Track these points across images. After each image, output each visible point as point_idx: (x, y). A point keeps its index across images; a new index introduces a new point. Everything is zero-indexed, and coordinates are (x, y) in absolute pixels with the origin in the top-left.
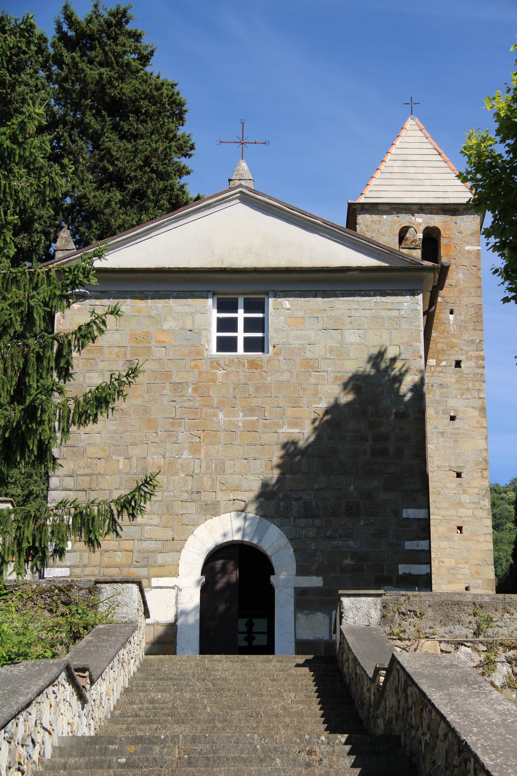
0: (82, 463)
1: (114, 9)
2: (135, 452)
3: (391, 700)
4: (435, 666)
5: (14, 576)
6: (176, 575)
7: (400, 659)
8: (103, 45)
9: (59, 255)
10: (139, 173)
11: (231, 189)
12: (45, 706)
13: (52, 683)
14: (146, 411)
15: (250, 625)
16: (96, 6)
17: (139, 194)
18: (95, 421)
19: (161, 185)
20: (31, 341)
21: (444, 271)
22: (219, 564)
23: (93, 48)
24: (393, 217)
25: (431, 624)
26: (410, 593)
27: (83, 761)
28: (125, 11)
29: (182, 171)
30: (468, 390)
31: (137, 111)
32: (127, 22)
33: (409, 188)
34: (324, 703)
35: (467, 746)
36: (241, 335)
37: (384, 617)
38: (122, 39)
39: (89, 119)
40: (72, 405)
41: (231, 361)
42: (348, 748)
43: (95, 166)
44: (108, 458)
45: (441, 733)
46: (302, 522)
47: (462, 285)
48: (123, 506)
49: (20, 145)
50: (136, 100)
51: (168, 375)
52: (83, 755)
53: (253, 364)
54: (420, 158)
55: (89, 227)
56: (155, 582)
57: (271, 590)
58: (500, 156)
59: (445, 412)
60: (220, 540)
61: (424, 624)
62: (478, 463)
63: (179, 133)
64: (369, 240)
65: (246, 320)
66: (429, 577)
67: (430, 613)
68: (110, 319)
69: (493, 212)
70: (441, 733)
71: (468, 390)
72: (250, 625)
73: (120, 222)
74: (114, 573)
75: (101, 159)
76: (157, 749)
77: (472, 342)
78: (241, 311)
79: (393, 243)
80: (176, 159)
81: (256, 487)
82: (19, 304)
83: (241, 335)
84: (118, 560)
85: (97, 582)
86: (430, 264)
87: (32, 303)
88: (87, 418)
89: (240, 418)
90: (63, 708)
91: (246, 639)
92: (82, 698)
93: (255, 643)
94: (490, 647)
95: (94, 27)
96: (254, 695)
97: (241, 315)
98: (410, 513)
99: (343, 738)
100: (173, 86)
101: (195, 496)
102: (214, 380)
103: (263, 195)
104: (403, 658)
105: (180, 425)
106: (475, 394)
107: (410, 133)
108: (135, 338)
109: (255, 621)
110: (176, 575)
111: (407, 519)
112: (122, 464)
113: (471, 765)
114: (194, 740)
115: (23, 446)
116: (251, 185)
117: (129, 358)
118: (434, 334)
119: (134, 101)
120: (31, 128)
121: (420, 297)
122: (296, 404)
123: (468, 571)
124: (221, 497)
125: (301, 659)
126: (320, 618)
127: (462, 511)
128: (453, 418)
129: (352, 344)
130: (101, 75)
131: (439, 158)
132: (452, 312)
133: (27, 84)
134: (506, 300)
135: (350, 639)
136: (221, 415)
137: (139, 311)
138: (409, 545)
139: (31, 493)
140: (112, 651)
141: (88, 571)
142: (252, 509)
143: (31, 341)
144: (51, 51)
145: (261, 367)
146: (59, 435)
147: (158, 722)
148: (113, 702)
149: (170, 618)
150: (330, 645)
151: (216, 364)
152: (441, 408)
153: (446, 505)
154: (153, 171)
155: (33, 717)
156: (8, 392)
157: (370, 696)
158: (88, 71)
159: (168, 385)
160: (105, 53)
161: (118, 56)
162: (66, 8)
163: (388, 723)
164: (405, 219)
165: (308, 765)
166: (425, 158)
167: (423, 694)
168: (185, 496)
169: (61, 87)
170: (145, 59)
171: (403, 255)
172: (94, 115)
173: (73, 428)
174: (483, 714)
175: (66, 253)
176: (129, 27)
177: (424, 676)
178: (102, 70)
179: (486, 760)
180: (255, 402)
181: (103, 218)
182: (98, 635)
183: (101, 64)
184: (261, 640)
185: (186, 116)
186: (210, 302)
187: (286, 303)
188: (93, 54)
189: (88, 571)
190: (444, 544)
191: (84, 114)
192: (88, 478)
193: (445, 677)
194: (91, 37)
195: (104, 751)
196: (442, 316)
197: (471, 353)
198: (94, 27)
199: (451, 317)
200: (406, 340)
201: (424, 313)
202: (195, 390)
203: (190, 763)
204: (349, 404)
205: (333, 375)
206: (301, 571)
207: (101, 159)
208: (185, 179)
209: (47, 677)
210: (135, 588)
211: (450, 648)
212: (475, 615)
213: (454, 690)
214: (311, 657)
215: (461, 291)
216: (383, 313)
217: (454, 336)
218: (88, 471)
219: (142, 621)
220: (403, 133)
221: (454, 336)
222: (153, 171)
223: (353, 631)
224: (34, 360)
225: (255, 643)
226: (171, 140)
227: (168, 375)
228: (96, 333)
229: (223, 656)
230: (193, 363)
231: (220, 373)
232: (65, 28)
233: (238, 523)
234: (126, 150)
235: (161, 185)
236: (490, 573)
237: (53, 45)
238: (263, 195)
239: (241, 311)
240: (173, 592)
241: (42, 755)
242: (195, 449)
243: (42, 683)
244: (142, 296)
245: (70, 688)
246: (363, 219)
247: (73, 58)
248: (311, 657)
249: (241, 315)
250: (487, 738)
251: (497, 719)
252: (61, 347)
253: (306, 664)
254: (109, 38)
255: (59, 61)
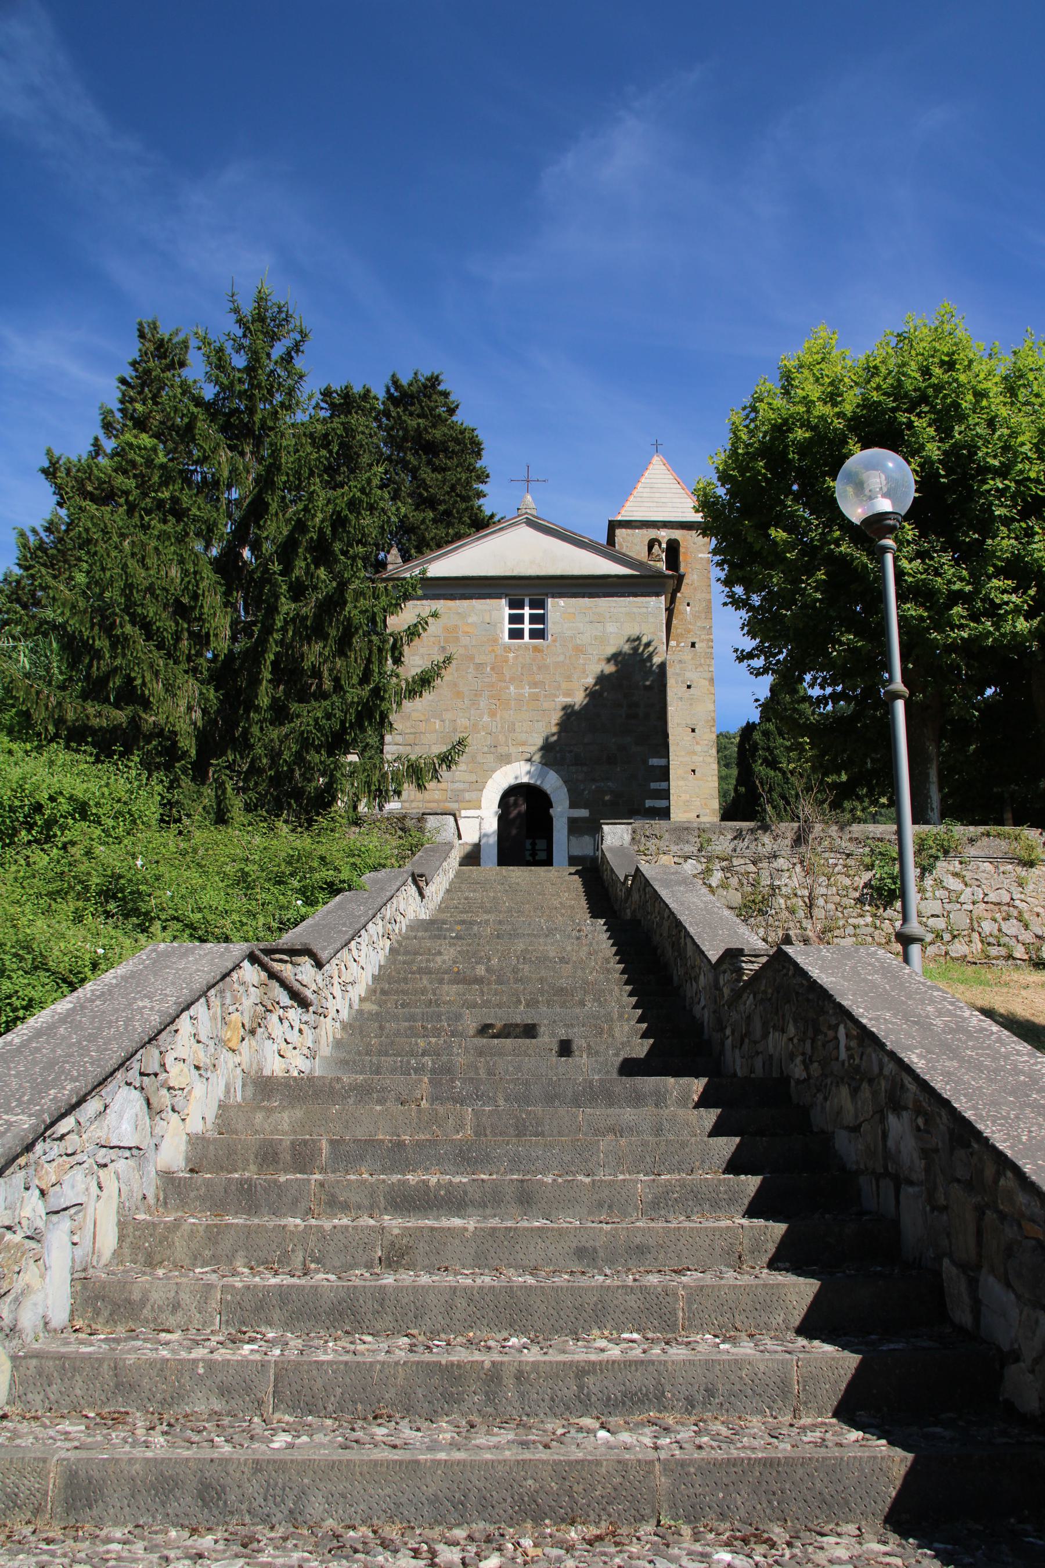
0: (408, 724)
1: (429, 375)
2: (448, 716)
3: (635, 896)
4: (665, 873)
5: (366, 809)
6: (479, 808)
7: (641, 869)
8: (420, 402)
9: (390, 567)
10: (447, 497)
11: (519, 516)
12: (401, 898)
13: (404, 884)
14: (455, 685)
15: (534, 844)
16: (416, 374)
17: (447, 513)
18: (421, 696)
19: (464, 506)
20: (374, 638)
21: (680, 578)
22: (512, 799)
23: (413, 404)
24: (644, 531)
25: (667, 844)
26: (652, 822)
27: (427, 934)
28: (437, 377)
29: (480, 495)
30: (701, 665)
31: (446, 450)
32: (439, 384)
33: (655, 509)
34: (589, 900)
35: (680, 922)
36: (527, 626)
37: (633, 839)
38: (434, 397)
39: (409, 457)
40: (403, 685)
41: (520, 647)
42: (605, 928)
43: (414, 492)
44: (427, 720)
45: (666, 916)
46: (573, 769)
47: (696, 584)
48: (443, 760)
49: (367, 495)
50: (446, 442)
51: (471, 658)
52: (426, 931)
53: (536, 649)
54: (664, 486)
55: (409, 540)
56: (464, 813)
57: (550, 819)
58: (720, 496)
59: (683, 682)
60: (513, 782)
61: (662, 844)
62: (707, 721)
63: (478, 466)
64: (624, 555)
65: (531, 615)
66: (668, 808)
67: (666, 836)
68: (430, 620)
69: (716, 537)
70: (666, 916)
71: (701, 665)
72: (534, 844)
73: (432, 534)
74: (433, 807)
75: (418, 487)
76: (476, 928)
77: (704, 628)
78: (527, 608)
79: (642, 554)
80: (475, 486)
81: (540, 742)
82: (367, 611)
83: (527, 626)
84: (437, 797)
85: (423, 814)
86: (671, 573)
87: (375, 610)
88: (415, 693)
89: (527, 690)
90: (411, 900)
91: (531, 855)
92: (422, 895)
93: (537, 858)
94: (709, 859)
95: (414, 389)
96: (539, 894)
97: (527, 611)
98: (654, 762)
99: (602, 921)
100: (473, 430)
101: (493, 749)
102: (506, 662)
103: (544, 520)
104: (645, 868)
105: (481, 695)
106: (706, 668)
107: (656, 467)
108: (446, 629)
109: (537, 841)
110: (479, 808)
111: (653, 766)
112: (438, 725)
113: (683, 934)
114: (500, 922)
115: (371, 717)
116: (534, 512)
117: (442, 644)
118: (674, 622)
119: (443, 443)
120: (376, 482)
121: (663, 597)
122: (569, 678)
123: (699, 803)
124: (513, 750)
125: (573, 869)
126: (587, 839)
127: (695, 758)
128: (689, 687)
129: (611, 633)
130: (418, 424)
131: (678, 486)
132: (688, 605)
133: (363, 433)
134: (725, 604)
135: (608, 855)
136: (512, 688)
137: (450, 609)
138: (654, 786)
139: (367, 744)
140: (438, 863)
141: (414, 805)
142: (537, 758)
143: (374, 638)
144: (382, 407)
145: (543, 651)
146: (394, 706)
147: (472, 912)
148: (439, 899)
149: (476, 840)
150: (594, 859)
151: (508, 649)
152: (680, 679)
153: (683, 753)
154: (457, 495)
155: (395, 905)
156: (358, 675)
157: (622, 894)
158: (409, 422)
159: (472, 666)
160: (422, 408)
161: (432, 409)
162: (393, 376)
163: (634, 912)
164: (653, 533)
165: (578, 938)
166: (668, 486)
167: (655, 891)
168: (486, 749)
169: (388, 434)
170: (452, 411)
171: (650, 566)
172: (413, 454)
173: (405, 702)
174: (693, 903)
175: (395, 566)
176: (440, 388)
177: (656, 880)
178: (420, 420)
179: (691, 930)
180: (538, 678)
181: (420, 532)
182: (427, 851)
183: (419, 416)
184: (542, 856)
185: (483, 453)
186: (503, 602)
187: (561, 602)
188: (413, 408)
189: (414, 805)
190: (681, 783)
191: (406, 454)
192: (412, 736)
193: (671, 880)
194: (412, 396)
195: (440, 929)
196: (681, 607)
197: (703, 637)
198: (414, 389)
199: (688, 608)
200: (652, 630)
201: (666, 610)
202: (492, 669)
203: (498, 937)
204: (611, 674)
205: (597, 657)
206: (573, 805)
207: (418, 487)
208: (482, 501)
209: (401, 880)
210: (451, 818)
211: (681, 861)
212: (699, 837)
213: (676, 888)
214: (580, 868)
215: (695, 589)
216: (635, 610)
217: (690, 623)
218: (413, 730)
219: (457, 842)
220: (651, 467)
221: (690, 623)
222: (457, 495)
223: (611, 849)
224: (376, 651)
225: (537, 858)
226: (471, 471)
227: (471, 658)
228: (421, 631)
229: (516, 868)
230: (490, 648)
231: (511, 655)
232: (392, 390)
233: (525, 767)
234: (437, 480)
235: (464, 506)
236: (715, 804)
237: (383, 403)
238: (544, 520)
239: (527, 608)
240: (478, 821)
241: (400, 930)
242: (492, 714)
243: (398, 884)
244: (452, 597)
245: (414, 888)
246: (620, 533)
247: (398, 413)
248: (580, 868)
249: (527, 611)
250: (693, 917)
251: (702, 905)
252: (395, 641)
253: (577, 873)
254: (425, 396)
255: (388, 415)
